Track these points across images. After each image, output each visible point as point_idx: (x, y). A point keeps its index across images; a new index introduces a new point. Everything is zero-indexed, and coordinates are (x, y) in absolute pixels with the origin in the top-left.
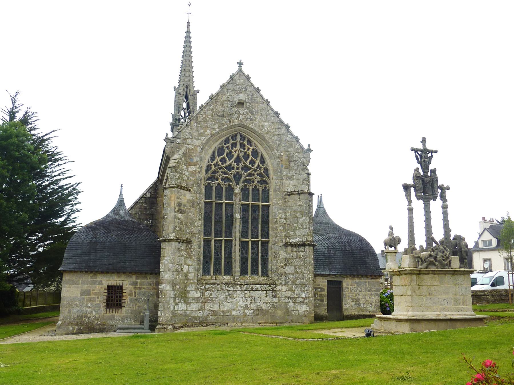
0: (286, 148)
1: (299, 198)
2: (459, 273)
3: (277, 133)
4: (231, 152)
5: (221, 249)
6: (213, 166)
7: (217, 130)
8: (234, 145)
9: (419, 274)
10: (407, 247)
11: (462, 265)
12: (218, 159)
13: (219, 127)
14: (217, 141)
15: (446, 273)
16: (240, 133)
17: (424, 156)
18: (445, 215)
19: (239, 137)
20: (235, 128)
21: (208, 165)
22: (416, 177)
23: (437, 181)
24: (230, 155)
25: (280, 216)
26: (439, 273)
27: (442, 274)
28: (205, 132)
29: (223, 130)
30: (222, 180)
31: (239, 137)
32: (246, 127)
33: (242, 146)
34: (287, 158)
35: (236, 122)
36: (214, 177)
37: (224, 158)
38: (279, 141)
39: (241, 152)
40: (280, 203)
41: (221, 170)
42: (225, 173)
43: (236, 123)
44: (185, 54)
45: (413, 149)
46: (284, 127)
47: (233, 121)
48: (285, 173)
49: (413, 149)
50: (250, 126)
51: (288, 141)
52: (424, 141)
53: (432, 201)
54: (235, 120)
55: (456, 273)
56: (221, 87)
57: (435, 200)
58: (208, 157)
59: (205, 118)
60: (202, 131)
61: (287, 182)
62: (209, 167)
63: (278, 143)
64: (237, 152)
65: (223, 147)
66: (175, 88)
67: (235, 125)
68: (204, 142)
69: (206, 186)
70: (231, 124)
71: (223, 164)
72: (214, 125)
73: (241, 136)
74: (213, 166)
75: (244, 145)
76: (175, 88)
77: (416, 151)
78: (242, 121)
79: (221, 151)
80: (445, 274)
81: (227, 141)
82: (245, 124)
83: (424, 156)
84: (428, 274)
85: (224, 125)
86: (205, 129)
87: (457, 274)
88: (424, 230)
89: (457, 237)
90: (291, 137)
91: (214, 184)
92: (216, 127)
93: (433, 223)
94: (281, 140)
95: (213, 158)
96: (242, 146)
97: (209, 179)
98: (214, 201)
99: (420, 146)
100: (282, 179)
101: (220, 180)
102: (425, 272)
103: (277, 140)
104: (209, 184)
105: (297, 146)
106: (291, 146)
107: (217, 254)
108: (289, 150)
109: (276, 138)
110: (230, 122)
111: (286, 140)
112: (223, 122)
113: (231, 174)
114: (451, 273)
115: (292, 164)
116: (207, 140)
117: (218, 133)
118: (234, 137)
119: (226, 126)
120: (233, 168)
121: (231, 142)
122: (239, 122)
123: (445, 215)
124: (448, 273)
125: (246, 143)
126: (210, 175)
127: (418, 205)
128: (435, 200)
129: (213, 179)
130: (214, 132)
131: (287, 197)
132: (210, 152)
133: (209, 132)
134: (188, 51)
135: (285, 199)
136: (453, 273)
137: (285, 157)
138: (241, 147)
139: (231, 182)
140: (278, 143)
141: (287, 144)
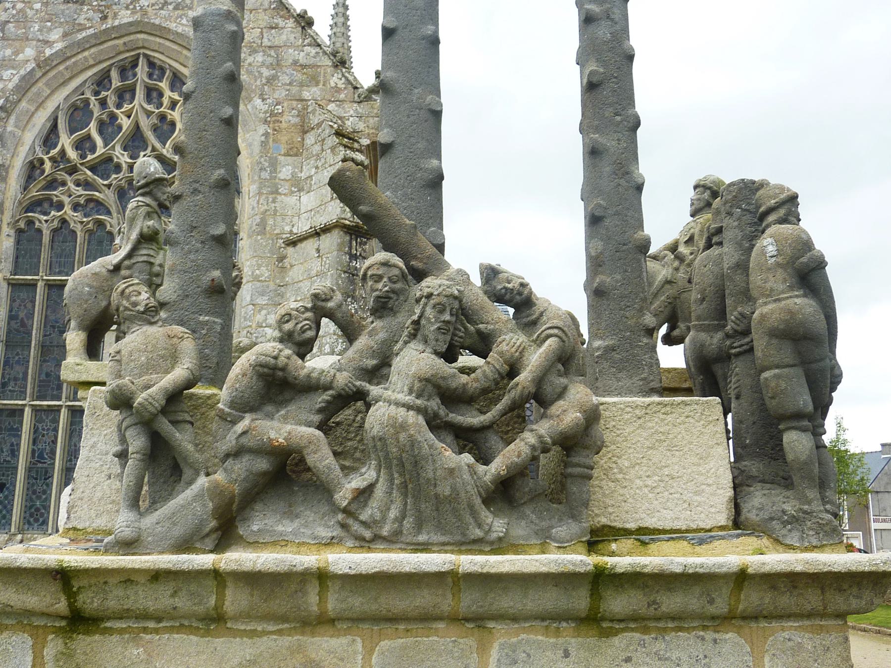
0: (295, 90)
1: (318, 251)
2: (671, 602)
3: (266, 42)
4: (113, 117)
5: (55, 442)
6: (48, 166)
7: (59, 46)
8: (125, 94)
9: (79, 622)
11: (759, 501)
12: (66, 141)
13: (65, 35)
14: (64, 83)
15: (469, 601)
16: (145, 55)
19: (142, 70)
20: (126, 39)
21: (31, 162)
24: (108, 126)
25: (259, 318)
26: (357, 602)
27: (426, 618)
28: (16, 53)
29: (83, 46)
30: (76, 207)
31: (142, 70)
32: (161, 32)
33: (153, 95)
34: (296, 120)
35: (125, 17)
36: (49, 199)
37: (88, 137)
38: (270, 66)
39: (149, 114)
40: (265, 272)
41: (75, 176)
42: (87, 185)
43: (125, 21)
44: (334, 30)
46: (291, 23)
47: (115, 15)
48: (285, 172)
50: (172, 26)
51: (303, 66)
54: (123, 12)
55: (618, 603)
58: (30, 137)
59: (21, 10)
60: (8, 52)
61: (292, 200)
62: (33, 168)
63: (266, 73)
64: (134, 113)
65: (87, 102)
67: (120, 26)
68: (11, 86)
69: (20, 231)
70: (109, 23)
71: (83, 156)
72: (50, 30)
73: (151, 64)
74: (48, 166)
75: (161, 95)
78: (145, 13)
79: (78, 113)
80: (478, 621)
81: (102, 81)
82: (157, 22)
84: (214, 621)
85: (83, 28)
86: (17, 44)
87: (638, 621)
89: (742, 210)
90: (313, 51)
91: (45, 222)
92: (55, 35)
94: (278, 64)
95: (50, 138)
96: (153, 95)
97: (35, 205)
98: (42, 277)
100: (276, 192)
101: (67, 208)
102: (159, 599)
103: (263, 64)
104: (30, 222)
105: (336, 80)
106: (314, 80)
107: (41, 456)
108: (306, 95)
109: (259, 57)
110: (104, 18)
111: (295, 63)
112: (81, 20)
113: (109, 186)
114: (549, 599)
115: (310, 139)
116: (23, 78)
117: (62, 57)
118: (127, 69)
119: (92, 31)
120: (118, 168)
121: (116, 82)
122: (138, 17)
124: (507, 602)
125: (164, 85)
126: (34, 192)
129: (46, 205)
130: (48, 52)
131: (290, 250)
132: (41, 119)
133: (29, 52)
134: (340, 24)
135: (282, 259)
136: (581, 601)
137: (290, 119)
138: (149, 98)
139: (109, 213)
140: (266, 73)
141: (298, 76)
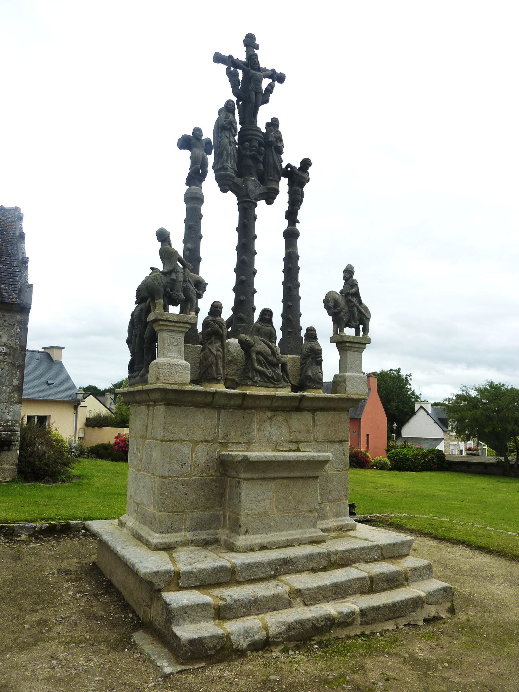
10: (199, 300)
17: (250, 81)
18: (291, 236)
22: (223, 126)
23: (279, 151)
45: (218, 58)
49: (218, 58)
52: (250, 42)
53: (261, 204)
56: (287, 217)
57: (270, 202)
66: (299, 223)
76: (299, 223)
77: (230, 62)
83: (250, 81)
88: (233, 276)
93: (259, 262)
99: (240, 54)
123: (291, 236)
127: (220, 208)
128: (270, 202)
